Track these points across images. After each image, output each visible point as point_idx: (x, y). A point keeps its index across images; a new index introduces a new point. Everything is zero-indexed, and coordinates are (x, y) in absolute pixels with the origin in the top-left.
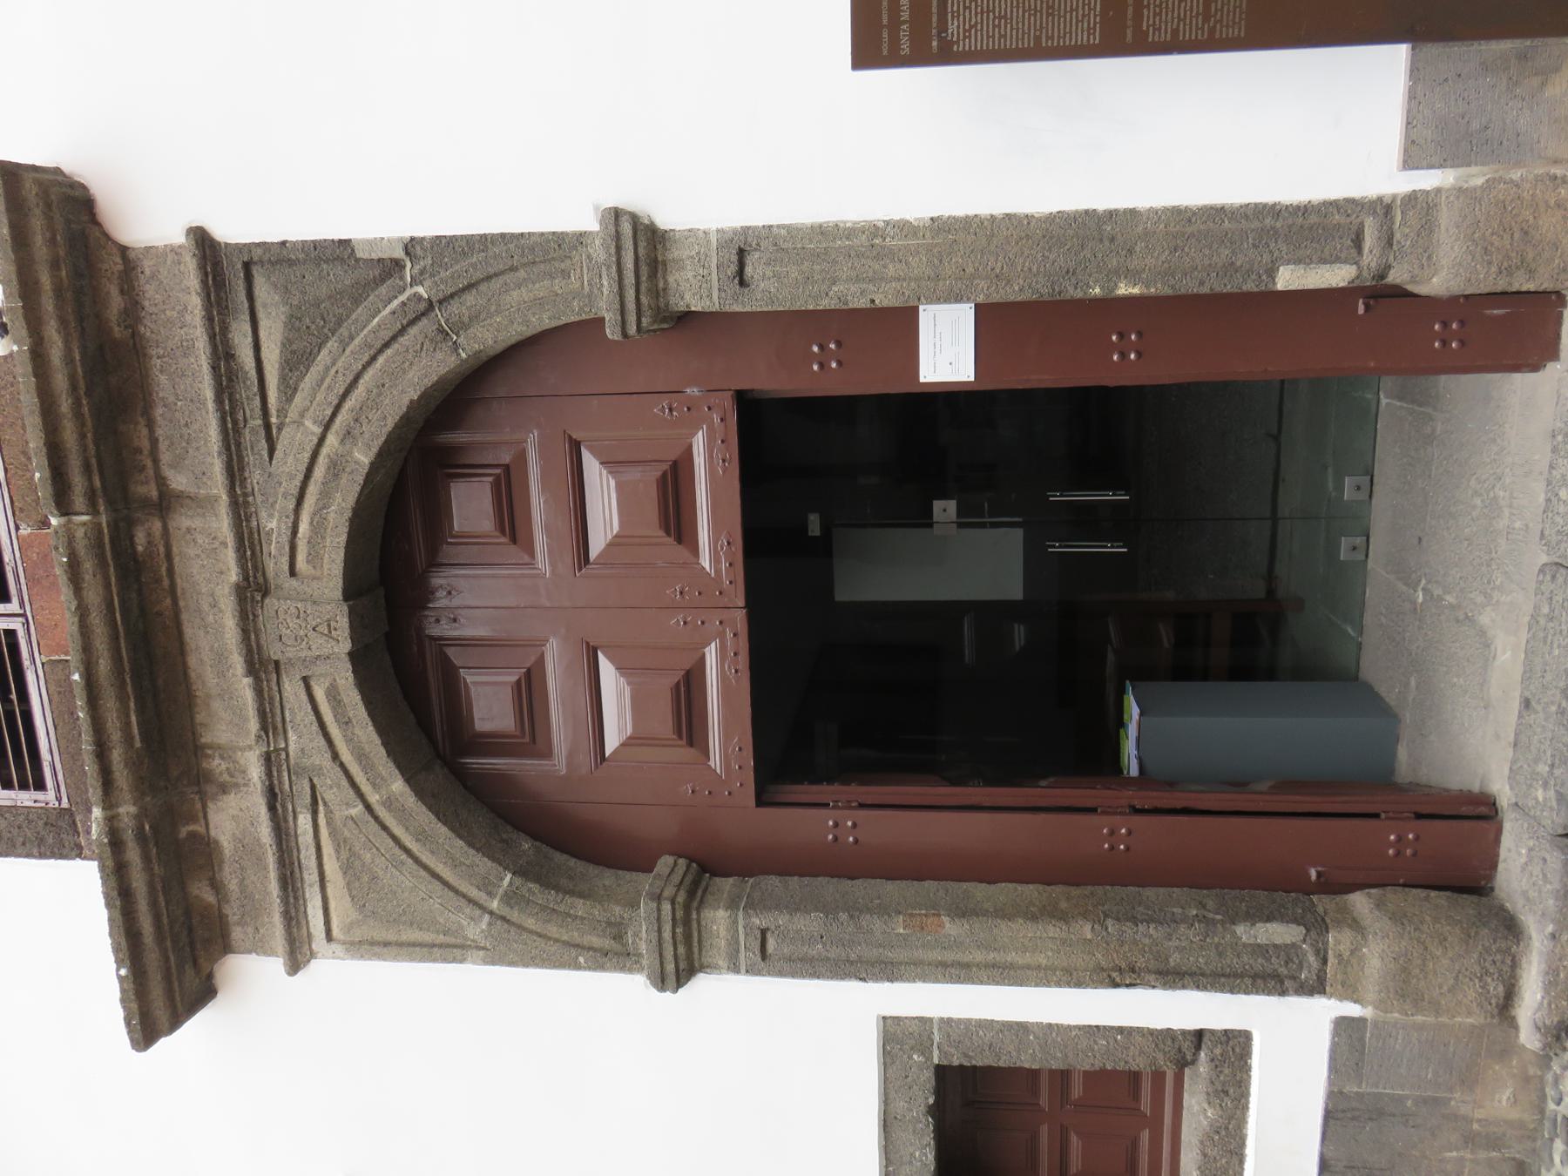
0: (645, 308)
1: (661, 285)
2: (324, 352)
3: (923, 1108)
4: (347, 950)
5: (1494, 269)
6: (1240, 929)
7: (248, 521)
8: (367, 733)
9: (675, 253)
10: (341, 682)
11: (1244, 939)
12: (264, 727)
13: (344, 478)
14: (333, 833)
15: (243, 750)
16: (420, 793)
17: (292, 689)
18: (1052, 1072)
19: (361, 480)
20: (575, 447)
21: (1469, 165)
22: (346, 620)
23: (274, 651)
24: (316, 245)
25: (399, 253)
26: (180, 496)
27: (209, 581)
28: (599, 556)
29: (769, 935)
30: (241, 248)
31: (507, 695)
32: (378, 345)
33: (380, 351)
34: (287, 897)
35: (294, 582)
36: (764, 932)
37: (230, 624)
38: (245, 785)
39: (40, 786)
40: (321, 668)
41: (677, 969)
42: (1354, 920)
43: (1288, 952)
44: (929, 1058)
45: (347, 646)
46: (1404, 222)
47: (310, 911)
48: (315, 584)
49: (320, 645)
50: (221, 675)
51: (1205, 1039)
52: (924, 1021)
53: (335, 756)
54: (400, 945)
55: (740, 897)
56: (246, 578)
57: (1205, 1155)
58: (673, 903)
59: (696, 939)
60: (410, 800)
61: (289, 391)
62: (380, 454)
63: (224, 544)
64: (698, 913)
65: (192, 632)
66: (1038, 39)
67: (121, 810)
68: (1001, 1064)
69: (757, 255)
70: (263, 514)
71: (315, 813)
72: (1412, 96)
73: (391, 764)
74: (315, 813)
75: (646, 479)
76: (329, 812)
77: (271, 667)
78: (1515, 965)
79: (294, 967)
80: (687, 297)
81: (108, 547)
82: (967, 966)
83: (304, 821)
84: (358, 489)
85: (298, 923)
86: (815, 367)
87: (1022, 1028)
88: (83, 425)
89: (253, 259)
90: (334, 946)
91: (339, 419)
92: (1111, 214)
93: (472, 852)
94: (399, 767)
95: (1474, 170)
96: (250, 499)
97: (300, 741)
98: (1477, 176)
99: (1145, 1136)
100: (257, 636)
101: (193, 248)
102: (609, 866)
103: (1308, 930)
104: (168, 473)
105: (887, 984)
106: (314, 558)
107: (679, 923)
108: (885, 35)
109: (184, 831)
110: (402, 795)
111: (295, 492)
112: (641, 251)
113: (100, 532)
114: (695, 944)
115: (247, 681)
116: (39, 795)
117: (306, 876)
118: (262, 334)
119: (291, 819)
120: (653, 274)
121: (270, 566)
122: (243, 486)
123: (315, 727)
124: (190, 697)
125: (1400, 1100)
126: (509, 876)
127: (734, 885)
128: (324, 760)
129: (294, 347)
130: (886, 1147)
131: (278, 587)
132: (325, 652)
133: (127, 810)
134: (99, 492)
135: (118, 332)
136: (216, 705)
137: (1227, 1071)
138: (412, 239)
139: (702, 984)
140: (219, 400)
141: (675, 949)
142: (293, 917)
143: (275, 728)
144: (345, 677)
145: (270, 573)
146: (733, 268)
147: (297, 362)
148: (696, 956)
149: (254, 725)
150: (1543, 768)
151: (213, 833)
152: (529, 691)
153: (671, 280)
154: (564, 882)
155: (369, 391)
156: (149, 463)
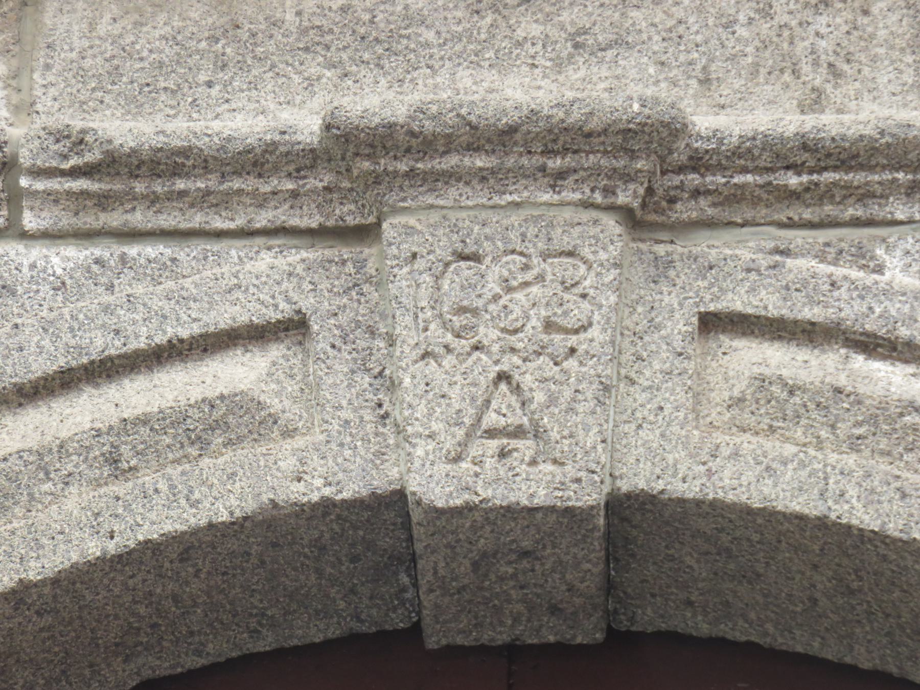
10: (286, 456)
12: (115, 164)
17: (260, 277)
22: (542, 497)
23: (414, 230)
27: (673, 36)
35: (680, 325)
37: (517, 90)
40: (342, 385)
45: (435, 483)
48: (675, 396)
56: (697, 162)
63: (815, 101)
77: (348, 213)
100: (483, 176)
106: (775, 405)
107: (875, 210)
115: (306, 124)
121: (743, 248)
123: (100, 344)
127: (707, 494)
131: (662, 269)
132: (413, 407)
143: (104, 201)
144: (311, 461)
145: (712, 246)
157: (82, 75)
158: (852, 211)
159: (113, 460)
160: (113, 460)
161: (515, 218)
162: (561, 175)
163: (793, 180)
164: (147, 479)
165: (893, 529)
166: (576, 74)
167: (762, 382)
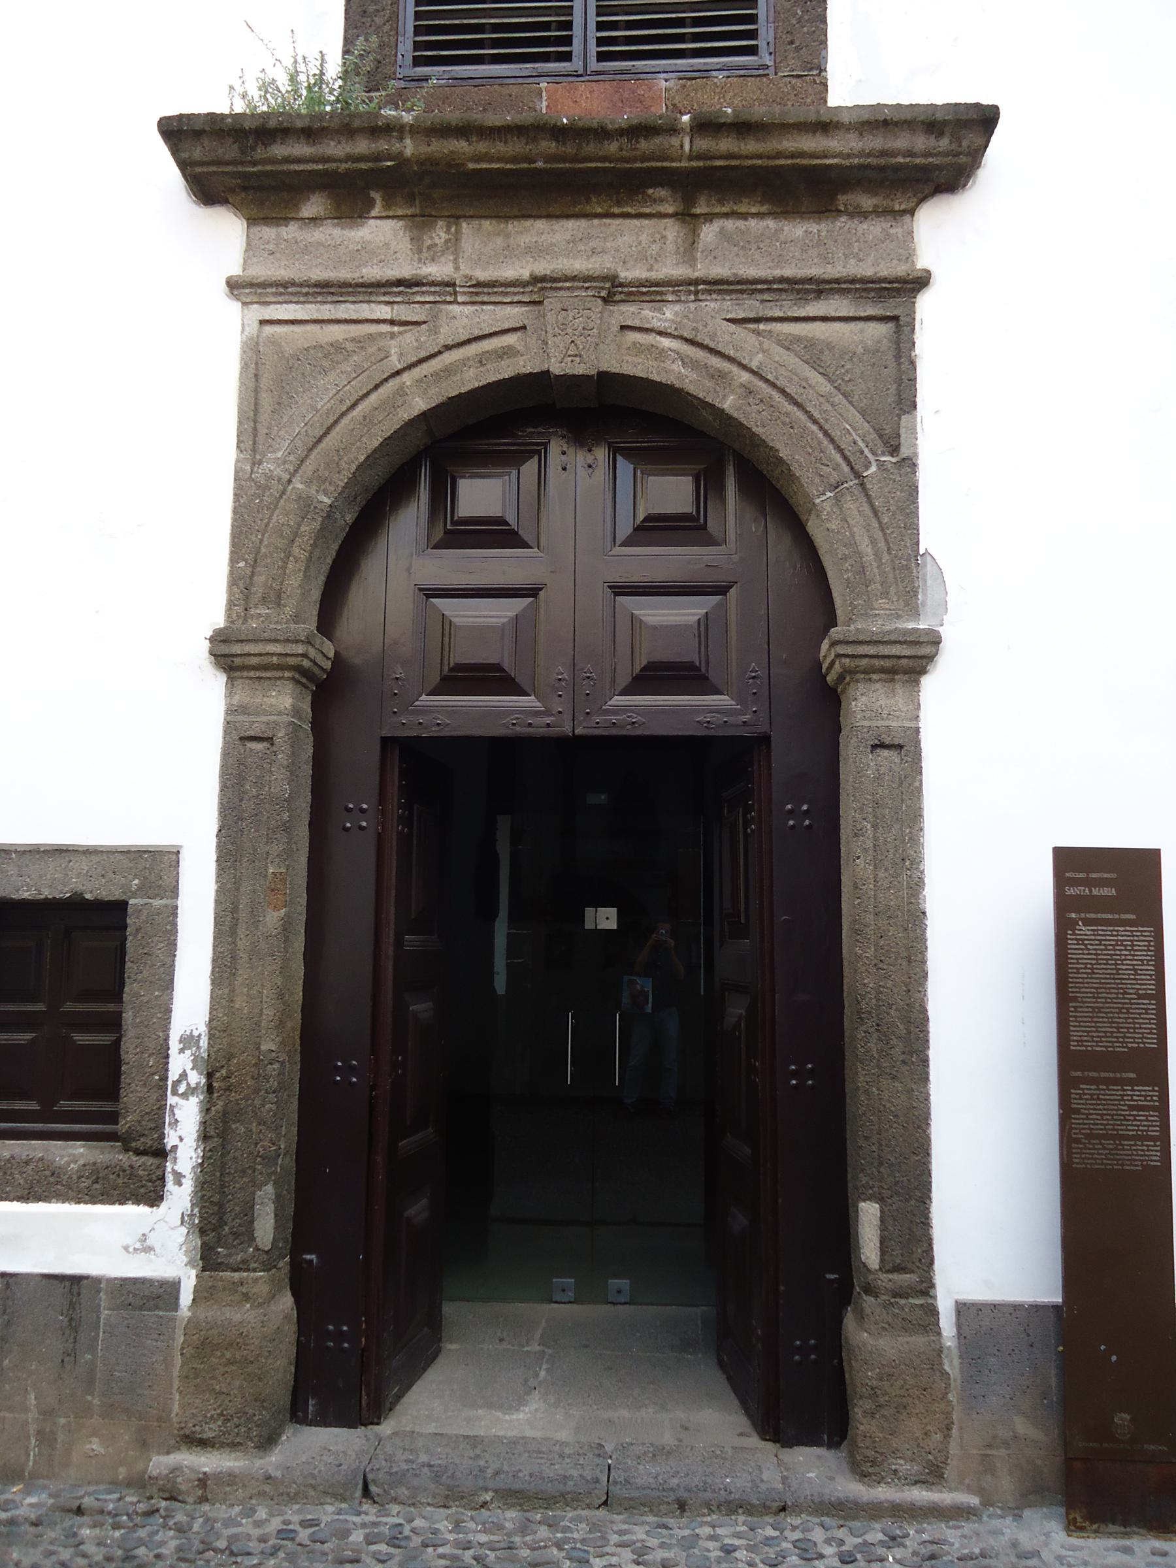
0: (858, 662)
1: (874, 677)
2: (820, 379)
3: (80, 888)
4: (251, 339)
5: (875, 1383)
6: (269, 1189)
7: (673, 292)
8: (471, 379)
9: (900, 690)
11: (259, 1193)
12: (479, 284)
13: (708, 383)
14: (371, 337)
15: (455, 261)
16: (411, 423)
17: (513, 314)
18: (119, 1015)
19: (709, 399)
20: (722, 590)
21: (961, 1357)
23: (553, 302)
24: (913, 380)
25: (905, 452)
29: (266, 744)
30: (911, 315)
31: (495, 511)
32: (827, 427)
33: (821, 428)
34: (308, 286)
35: (616, 328)
36: (270, 740)
37: (579, 265)
38: (420, 260)
39: (417, 62)
40: (533, 342)
41: (230, 654)
42: (274, 1296)
43: (246, 1234)
44: (134, 895)
45: (556, 369)
46: (913, 1306)
47: (292, 306)
48: (613, 346)
49: (557, 345)
51: (150, 1161)
52: (175, 892)
53: (448, 348)
54: (256, 391)
55: (300, 719)
56: (621, 285)
57: (27, 1163)
58: (304, 655)
59: (263, 675)
60: (406, 414)
61: (789, 344)
62: (730, 417)
63: (650, 269)
64: (288, 678)
65: (570, 227)
66: (1075, 999)
67: (408, 141)
68: (128, 965)
69: (897, 760)
70: (677, 307)
71: (392, 322)
72: (1016, 1307)
73: (441, 400)
74: (392, 322)
75: (689, 653)
76: (393, 335)
77: (536, 298)
78: (234, 1446)
79: (234, 286)
80: (864, 699)
81: (659, 164)
82: (233, 932)
83: (384, 312)
84: (701, 396)
85: (281, 294)
86: (789, 807)
87: (168, 985)
88: (769, 158)
89: (902, 328)
90: (256, 325)
91: (761, 384)
92: (925, 1062)
93: (354, 467)
95: (956, 1362)
96: (692, 297)
97: (462, 318)
98: (952, 1366)
99: (34, 1106)
101: (915, 274)
102: (323, 595)
103: (267, 1252)
104: (717, 225)
105: (215, 858)
106: (638, 349)
107: (664, 298)
108: (1081, 875)
109: (377, 196)
110: (410, 406)
111: (699, 339)
112: (904, 662)
113: (673, 160)
114: (258, 674)
115: (526, 275)
116: (409, 60)
117: (328, 306)
118: (837, 326)
119: (387, 298)
120: (883, 670)
123: (477, 332)
124: (508, 218)
125: (92, 1348)
126: (327, 501)
128: (446, 335)
129: (826, 353)
130: (67, 851)
133: (409, 147)
134: (708, 163)
135: (842, 199)
136: (499, 242)
137: (120, 1181)
138: (915, 465)
139: (219, 681)
140: (782, 280)
141: (255, 655)
142: (286, 289)
143: (477, 294)
145: (624, 307)
146: (887, 741)
147: (813, 353)
148: (245, 674)
149: (482, 275)
150: (423, 1458)
151: (372, 222)
152: (495, 534)
153: (878, 685)
154: (316, 554)
155: (787, 414)
156: (725, 210)
157: (471, 259)
158: (659, 298)
159: (481, 362)
160: (481, 362)
161: (576, 300)
162: (587, 288)
163: (644, 290)
164: (489, 366)
165: (664, 381)
166: (592, 260)
167: (634, 343)
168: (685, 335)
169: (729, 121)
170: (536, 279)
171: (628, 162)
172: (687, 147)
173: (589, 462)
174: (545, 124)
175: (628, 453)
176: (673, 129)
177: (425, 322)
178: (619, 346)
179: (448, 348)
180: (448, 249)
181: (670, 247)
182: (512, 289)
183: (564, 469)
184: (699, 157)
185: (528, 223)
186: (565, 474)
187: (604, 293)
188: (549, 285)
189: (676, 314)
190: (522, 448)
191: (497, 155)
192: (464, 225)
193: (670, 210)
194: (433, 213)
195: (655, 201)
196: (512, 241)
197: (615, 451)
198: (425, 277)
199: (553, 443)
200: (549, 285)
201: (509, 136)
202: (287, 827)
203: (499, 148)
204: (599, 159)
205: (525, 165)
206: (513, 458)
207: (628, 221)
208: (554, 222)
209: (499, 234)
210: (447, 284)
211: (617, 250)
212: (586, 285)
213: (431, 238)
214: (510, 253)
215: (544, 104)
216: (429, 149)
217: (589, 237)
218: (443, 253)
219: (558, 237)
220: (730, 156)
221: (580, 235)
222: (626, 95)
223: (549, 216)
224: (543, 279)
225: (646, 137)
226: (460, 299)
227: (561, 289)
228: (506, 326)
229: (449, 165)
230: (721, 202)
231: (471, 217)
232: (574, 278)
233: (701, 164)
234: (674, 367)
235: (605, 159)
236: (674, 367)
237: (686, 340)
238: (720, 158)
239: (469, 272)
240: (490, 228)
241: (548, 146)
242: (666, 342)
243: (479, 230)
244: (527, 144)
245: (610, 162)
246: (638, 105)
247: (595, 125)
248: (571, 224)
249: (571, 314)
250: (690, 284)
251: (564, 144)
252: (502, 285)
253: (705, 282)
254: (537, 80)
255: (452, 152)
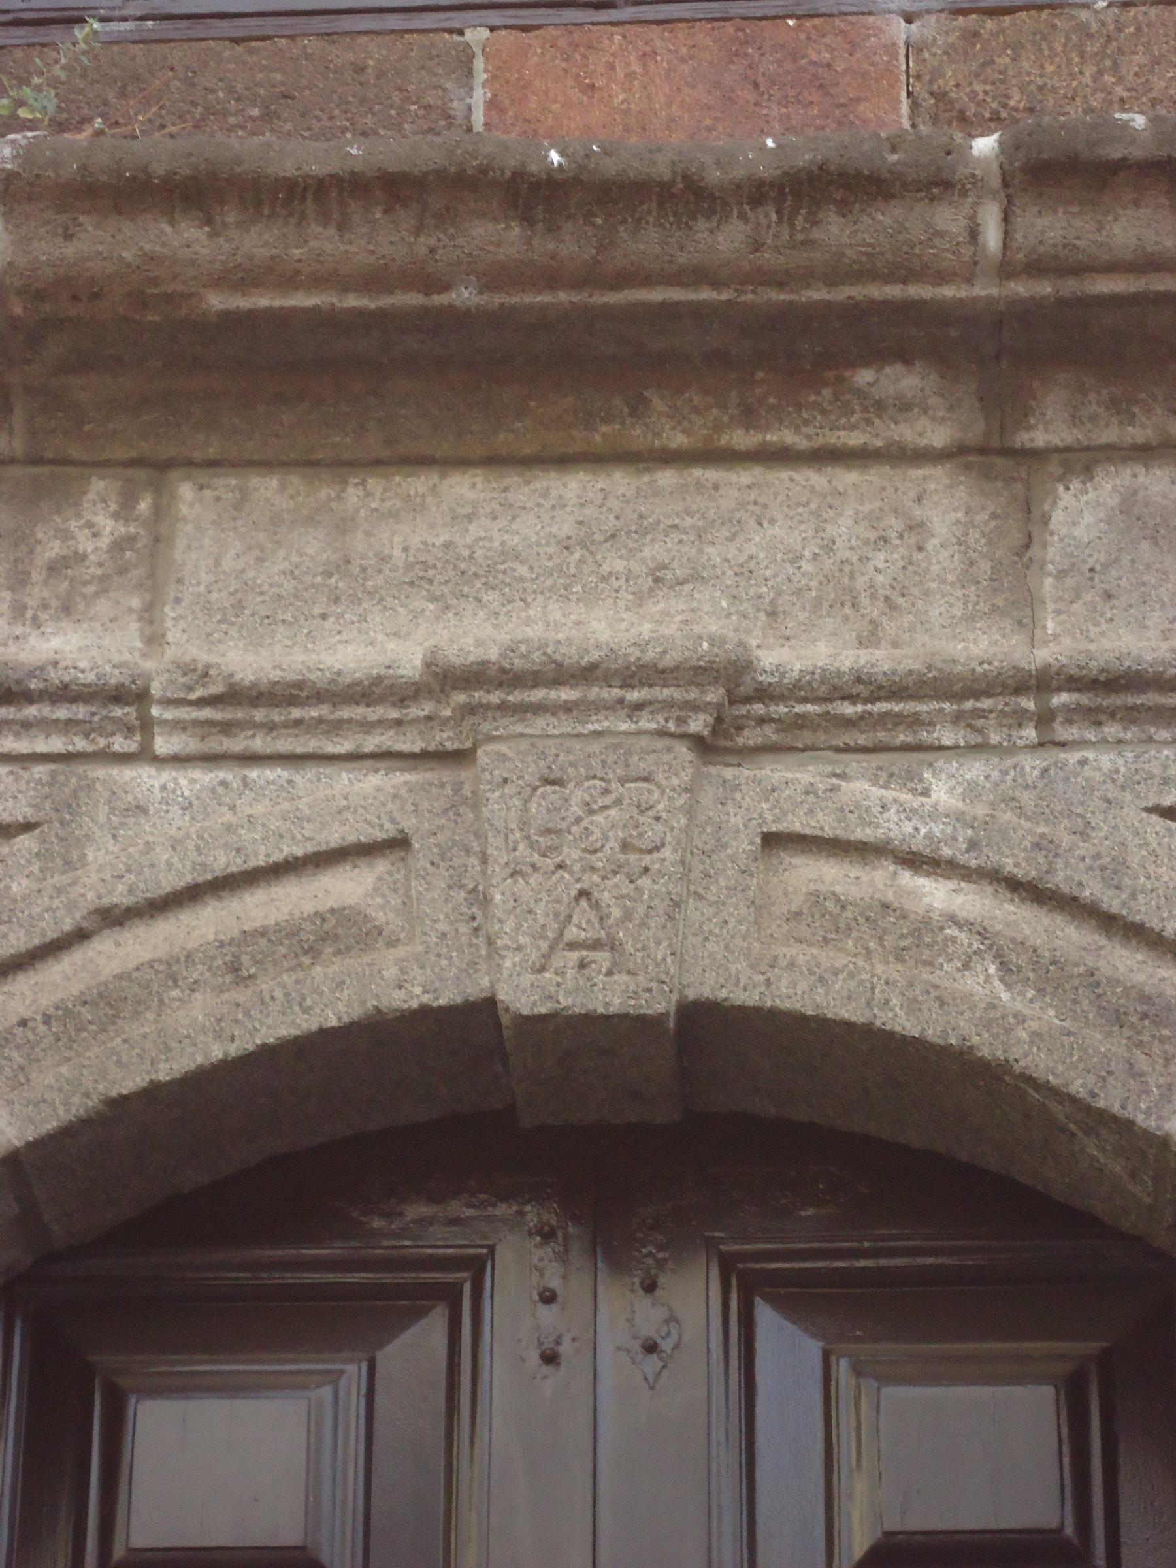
7: (957, 719)
8: (198, 1033)
10: (388, 964)
12: (234, 695)
15: (150, 614)
17: (361, 798)
19: (1110, 1100)
23: (508, 755)
26: (1029, 518)
28: (419, 1314)
35: (745, 844)
37: (604, 626)
45: (522, 992)
50: (420, 575)
53: (113, 918)
56: (763, 694)
63: (870, 638)
65: (563, 503)
70: (976, 770)
77: (446, 739)
81: (893, 291)
84: (1078, 1087)
94: (66, 1133)
104: (1109, 486)
106: (828, 918)
107: (924, 736)
111: (1060, 879)
113: (941, 278)
115: (407, 658)
122: (1073, 714)
123: (222, 862)
124: (344, 466)
128: (106, 867)
134: (1070, 286)
136: (314, 546)
143: (227, 728)
145: (774, 771)
149: (245, 661)
156: (1137, 434)
158: (902, 737)
161: (595, 747)
162: (639, 706)
163: (849, 710)
165: (932, 1034)
166: (654, 608)
167: (817, 899)
168: (1009, 865)
169: (1137, 153)
170: (445, 679)
171: (781, 285)
172: (992, 237)
173: (648, 1330)
174: (484, 171)
175: (802, 1296)
176: (941, 182)
177: (28, 827)
178: (759, 908)
179: (113, 918)
180: (122, 571)
181: (942, 558)
182: (359, 712)
183: (550, 1359)
184: (1036, 268)
185: (419, 484)
186: (550, 1382)
187: (698, 724)
188: (495, 698)
189: (972, 792)
190: (387, 1278)
191: (316, 268)
192: (186, 491)
193: (938, 436)
194: (74, 452)
195: (880, 406)
196: (358, 542)
197: (746, 1285)
198: (38, 671)
199: (505, 1255)
200: (495, 698)
201: (353, 206)
202: (822, 829)
203: (323, 242)
204: (676, 279)
205: (413, 299)
206: (357, 1316)
207: (782, 477)
208: (513, 479)
209: (311, 520)
210: (118, 696)
211: (745, 572)
212: (634, 696)
213: (65, 535)
214: (348, 585)
215: (479, 96)
216: (69, 250)
217: (643, 530)
218: (104, 584)
219: (528, 529)
220: (1150, 263)
221: (611, 523)
222: (768, 65)
223: (494, 461)
224: (474, 676)
225: (844, 208)
226: (162, 745)
227: (539, 709)
228: (335, 836)
229: (139, 300)
230: (1120, 408)
231: (212, 464)
232: (587, 674)
233: (1045, 288)
234: (972, 983)
235: (698, 276)
236: (972, 983)
237: (1015, 886)
238: (1113, 268)
239: (200, 654)
240: (282, 502)
241: (496, 237)
242: (936, 894)
243: (238, 506)
244: (418, 230)
245: (716, 284)
246: (815, 96)
247: (662, 170)
248: (574, 486)
249: (578, 796)
250: (1018, 690)
251: (553, 228)
252: (319, 696)
253: (1073, 683)
254: (456, 19)
255: (152, 258)
